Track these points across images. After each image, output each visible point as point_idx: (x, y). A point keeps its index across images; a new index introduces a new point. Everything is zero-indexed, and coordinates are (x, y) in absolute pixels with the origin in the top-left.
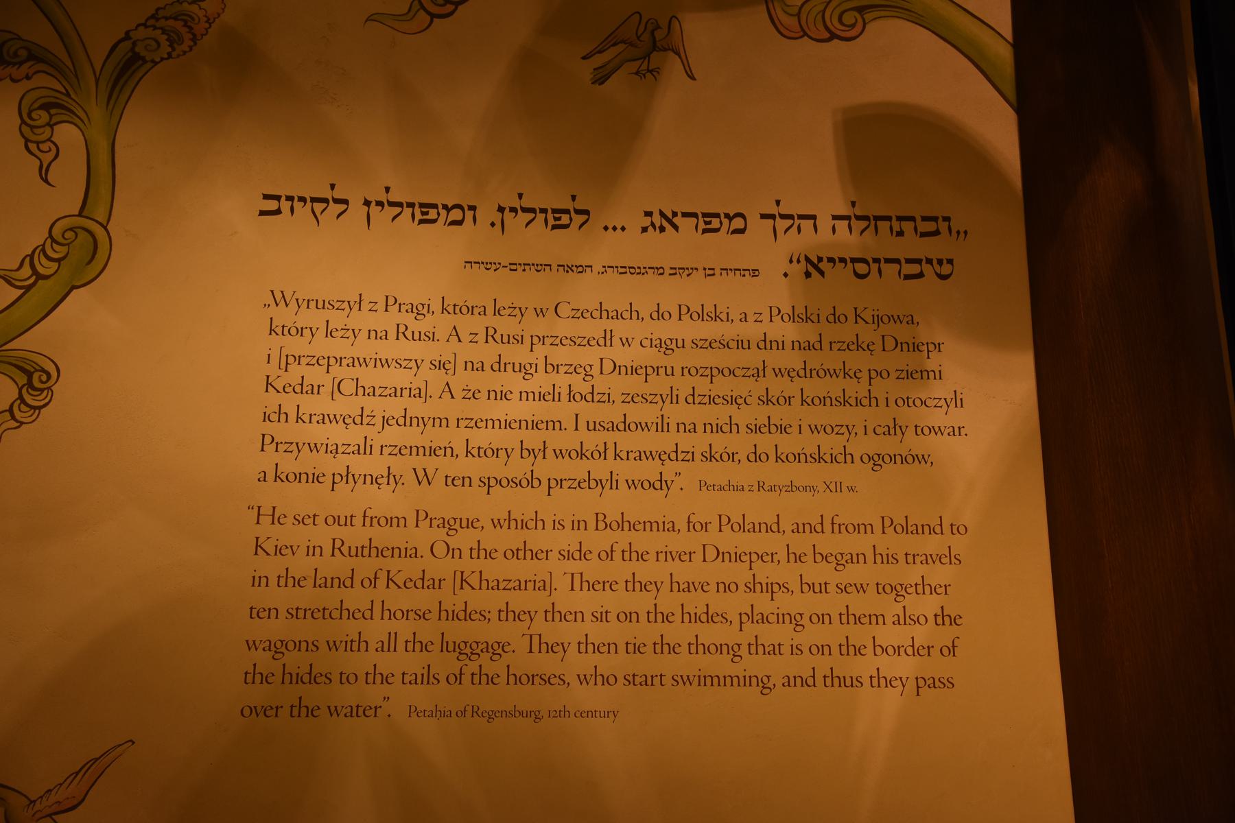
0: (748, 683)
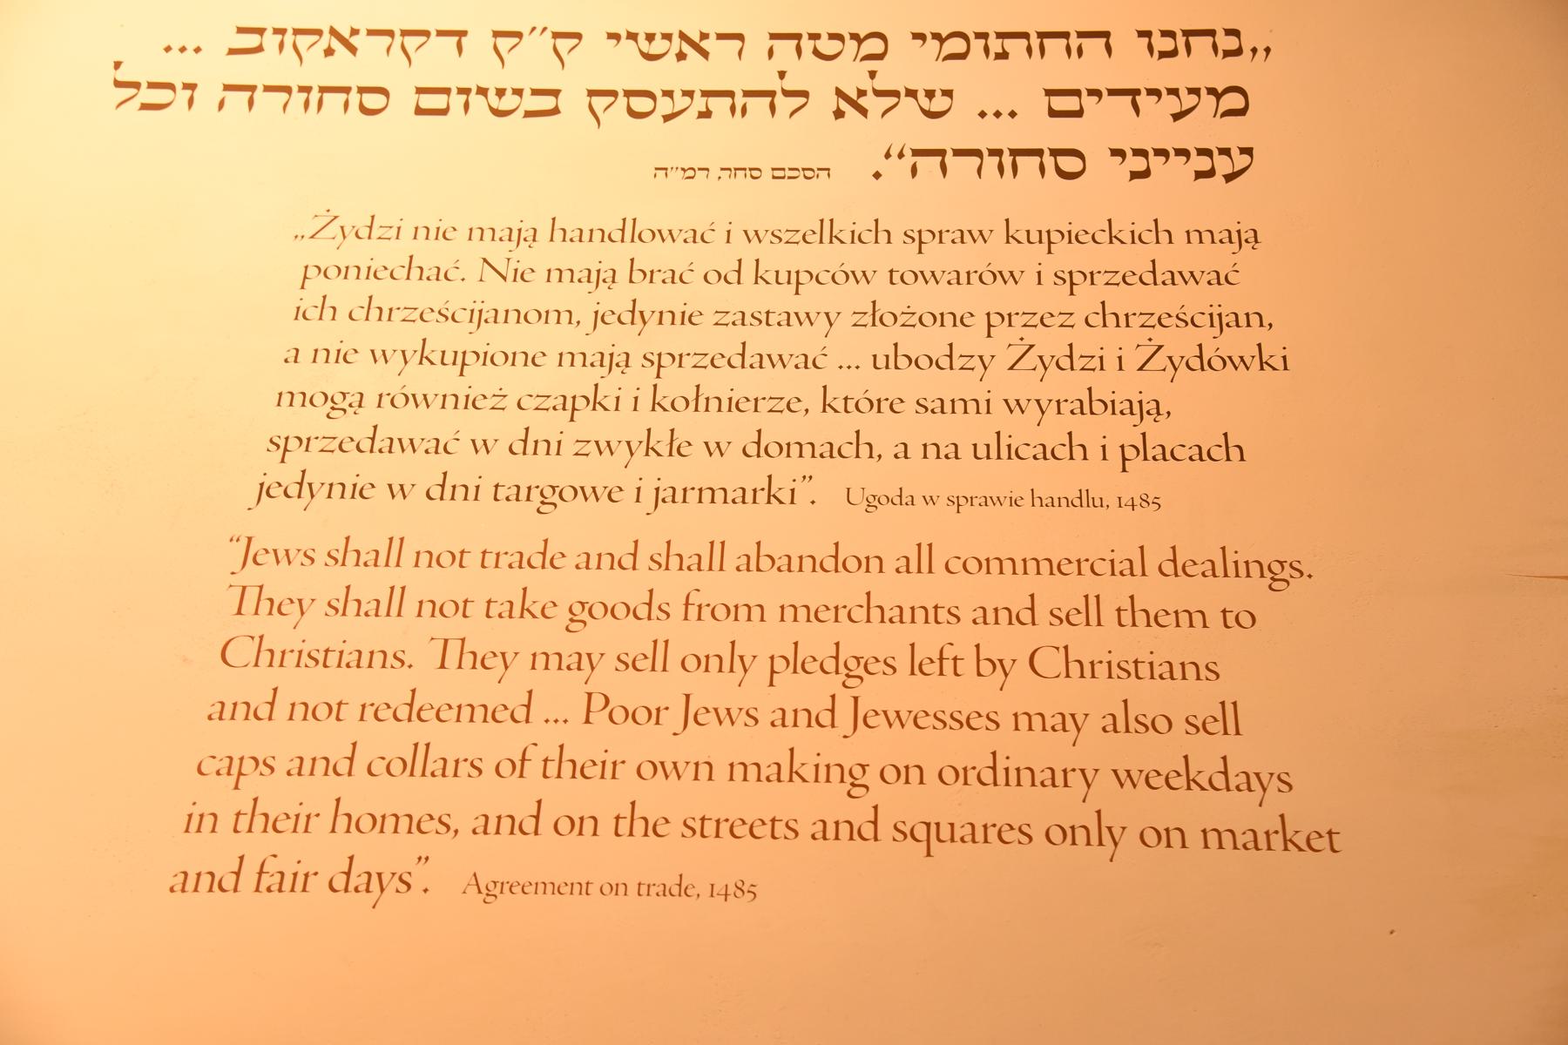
0: (1013, 780)
